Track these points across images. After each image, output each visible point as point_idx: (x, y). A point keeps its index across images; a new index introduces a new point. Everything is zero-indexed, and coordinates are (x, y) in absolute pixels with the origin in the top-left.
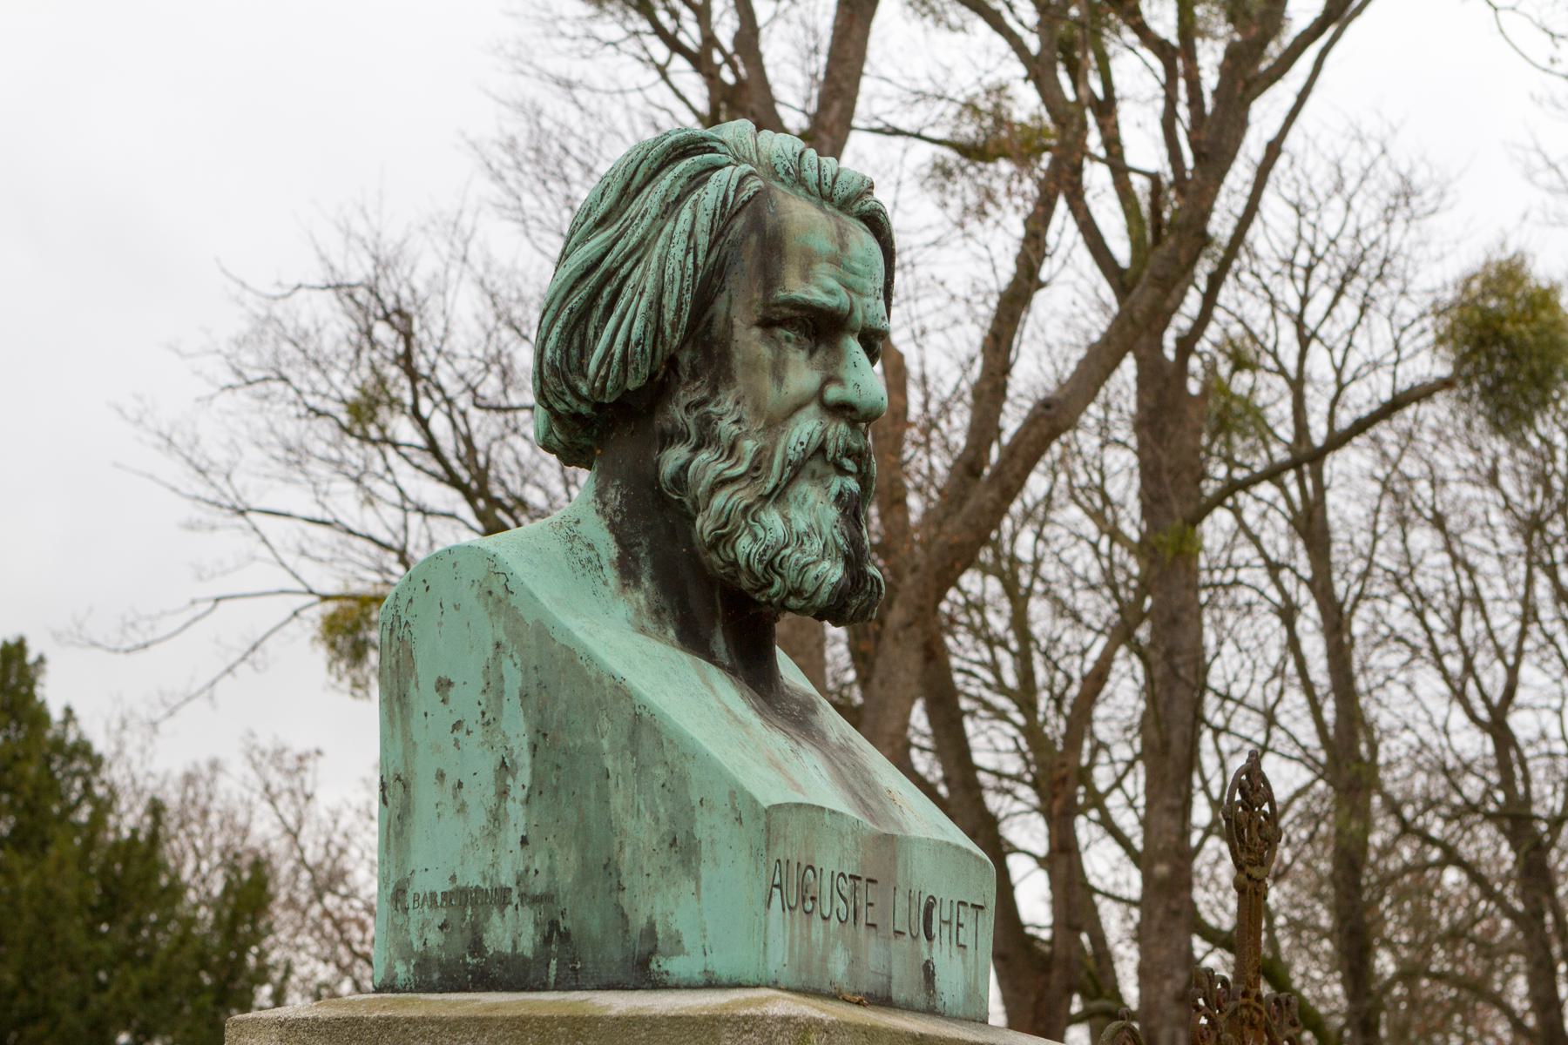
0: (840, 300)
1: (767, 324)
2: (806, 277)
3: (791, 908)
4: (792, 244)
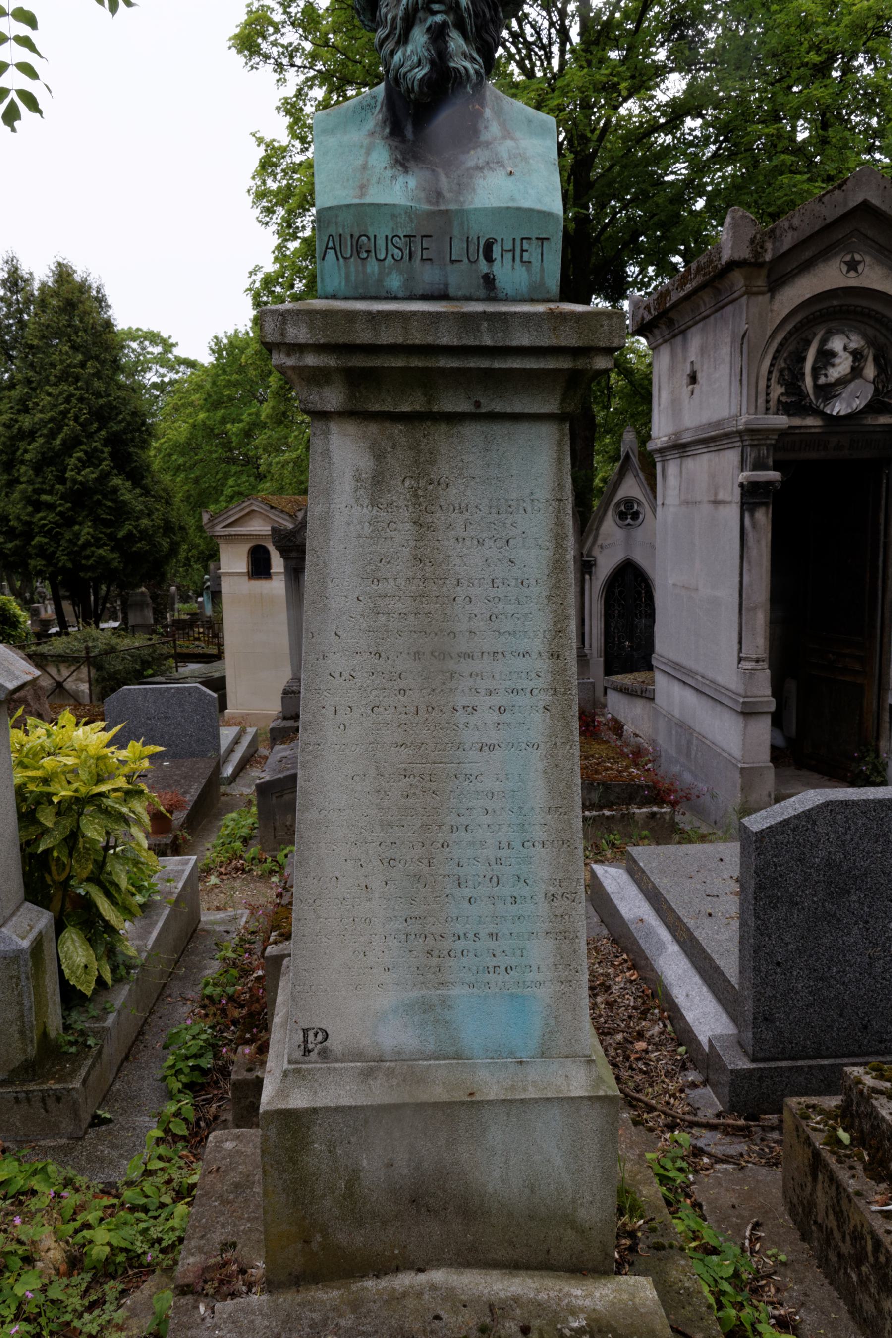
3: (345, 258)
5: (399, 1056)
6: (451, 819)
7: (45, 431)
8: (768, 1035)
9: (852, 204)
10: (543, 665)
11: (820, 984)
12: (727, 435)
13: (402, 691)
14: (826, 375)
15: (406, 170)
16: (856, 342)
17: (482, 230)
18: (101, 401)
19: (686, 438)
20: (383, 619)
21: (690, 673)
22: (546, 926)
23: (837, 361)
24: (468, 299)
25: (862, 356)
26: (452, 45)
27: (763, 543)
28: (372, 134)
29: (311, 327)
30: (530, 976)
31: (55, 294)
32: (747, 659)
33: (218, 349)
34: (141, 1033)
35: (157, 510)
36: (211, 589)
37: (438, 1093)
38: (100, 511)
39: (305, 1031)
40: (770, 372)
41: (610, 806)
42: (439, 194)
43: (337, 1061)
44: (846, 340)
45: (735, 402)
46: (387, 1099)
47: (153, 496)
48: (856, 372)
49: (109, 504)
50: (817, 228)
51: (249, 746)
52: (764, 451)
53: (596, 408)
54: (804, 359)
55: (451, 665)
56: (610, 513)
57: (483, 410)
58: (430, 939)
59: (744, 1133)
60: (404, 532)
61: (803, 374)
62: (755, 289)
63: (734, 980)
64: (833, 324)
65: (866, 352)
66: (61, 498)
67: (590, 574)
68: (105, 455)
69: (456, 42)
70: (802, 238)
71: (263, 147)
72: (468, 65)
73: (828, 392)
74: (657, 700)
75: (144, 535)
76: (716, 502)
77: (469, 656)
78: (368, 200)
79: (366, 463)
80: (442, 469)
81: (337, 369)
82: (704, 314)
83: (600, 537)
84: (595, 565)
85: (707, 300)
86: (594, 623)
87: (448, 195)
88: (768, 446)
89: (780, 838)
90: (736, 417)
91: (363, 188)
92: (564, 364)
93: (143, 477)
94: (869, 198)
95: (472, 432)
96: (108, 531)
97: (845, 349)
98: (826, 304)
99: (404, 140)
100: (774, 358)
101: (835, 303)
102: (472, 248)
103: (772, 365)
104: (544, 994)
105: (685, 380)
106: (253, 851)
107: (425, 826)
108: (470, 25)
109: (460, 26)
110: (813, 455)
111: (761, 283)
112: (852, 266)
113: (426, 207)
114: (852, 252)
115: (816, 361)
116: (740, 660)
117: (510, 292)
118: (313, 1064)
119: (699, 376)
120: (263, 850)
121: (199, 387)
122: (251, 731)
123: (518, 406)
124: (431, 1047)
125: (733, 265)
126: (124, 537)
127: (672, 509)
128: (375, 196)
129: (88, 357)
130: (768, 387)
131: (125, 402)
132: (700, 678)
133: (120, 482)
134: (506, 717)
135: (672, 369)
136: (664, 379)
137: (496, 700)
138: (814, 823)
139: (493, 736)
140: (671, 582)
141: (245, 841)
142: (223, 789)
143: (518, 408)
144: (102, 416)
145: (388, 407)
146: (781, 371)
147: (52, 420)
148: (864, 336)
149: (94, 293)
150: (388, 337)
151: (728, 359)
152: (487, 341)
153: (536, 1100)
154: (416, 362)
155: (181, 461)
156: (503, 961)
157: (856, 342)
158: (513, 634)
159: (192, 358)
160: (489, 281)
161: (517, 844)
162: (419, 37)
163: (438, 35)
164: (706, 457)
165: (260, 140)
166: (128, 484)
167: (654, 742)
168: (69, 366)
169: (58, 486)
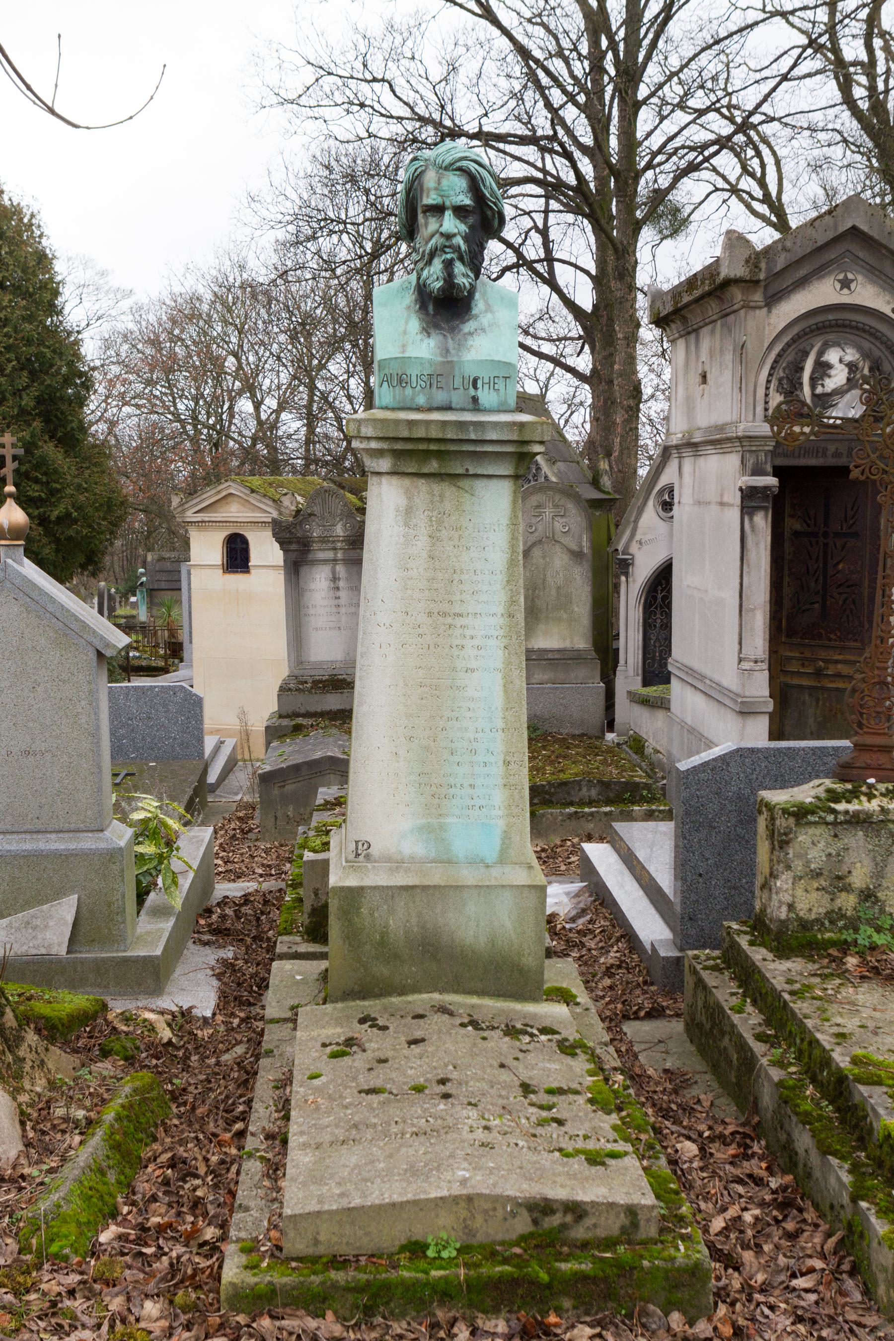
0: (439, 201)
1: (424, 212)
2: (428, 197)
4: (425, 187)
5: (412, 859)
8: (693, 932)
9: (842, 229)
11: (733, 892)
12: (729, 440)
13: (420, 635)
14: (823, 385)
15: (429, 335)
17: (471, 371)
18: (33, 349)
19: (698, 438)
20: (410, 592)
21: (702, 677)
23: (832, 372)
24: (463, 409)
25: (857, 369)
26: (456, 271)
27: (762, 546)
29: (375, 428)
39: (357, 842)
40: (768, 382)
41: (609, 802)
42: (447, 351)
43: (375, 861)
44: (842, 353)
48: (851, 383)
50: (809, 250)
54: (802, 369)
56: (651, 503)
57: (471, 473)
58: (434, 788)
60: (422, 544)
61: (801, 384)
62: (752, 304)
63: (672, 897)
64: (831, 337)
65: (861, 364)
67: (627, 575)
69: (459, 268)
72: (465, 281)
73: (824, 400)
74: (672, 709)
77: (460, 615)
78: (407, 355)
79: (402, 501)
81: (388, 450)
82: (712, 318)
84: (633, 564)
85: (714, 306)
86: (630, 633)
87: (453, 352)
90: (735, 424)
94: (857, 224)
97: (841, 361)
98: (820, 319)
99: (427, 314)
100: (772, 368)
101: (830, 317)
102: (466, 382)
103: (770, 375)
105: (699, 379)
107: (432, 717)
109: (461, 259)
113: (440, 359)
114: (845, 271)
115: (813, 372)
116: (740, 660)
119: (708, 376)
124: (433, 855)
125: (728, 283)
127: (687, 508)
128: (412, 352)
130: (767, 395)
132: (708, 682)
134: (481, 652)
137: (475, 642)
138: (728, 764)
146: (780, 380)
148: (860, 349)
151: (730, 366)
152: (473, 436)
153: (496, 887)
156: (477, 802)
157: (851, 355)
158: (487, 603)
160: (475, 400)
161: (487, 730)
162: (437, 266)
163: (448, 265)
164: (715, 457)
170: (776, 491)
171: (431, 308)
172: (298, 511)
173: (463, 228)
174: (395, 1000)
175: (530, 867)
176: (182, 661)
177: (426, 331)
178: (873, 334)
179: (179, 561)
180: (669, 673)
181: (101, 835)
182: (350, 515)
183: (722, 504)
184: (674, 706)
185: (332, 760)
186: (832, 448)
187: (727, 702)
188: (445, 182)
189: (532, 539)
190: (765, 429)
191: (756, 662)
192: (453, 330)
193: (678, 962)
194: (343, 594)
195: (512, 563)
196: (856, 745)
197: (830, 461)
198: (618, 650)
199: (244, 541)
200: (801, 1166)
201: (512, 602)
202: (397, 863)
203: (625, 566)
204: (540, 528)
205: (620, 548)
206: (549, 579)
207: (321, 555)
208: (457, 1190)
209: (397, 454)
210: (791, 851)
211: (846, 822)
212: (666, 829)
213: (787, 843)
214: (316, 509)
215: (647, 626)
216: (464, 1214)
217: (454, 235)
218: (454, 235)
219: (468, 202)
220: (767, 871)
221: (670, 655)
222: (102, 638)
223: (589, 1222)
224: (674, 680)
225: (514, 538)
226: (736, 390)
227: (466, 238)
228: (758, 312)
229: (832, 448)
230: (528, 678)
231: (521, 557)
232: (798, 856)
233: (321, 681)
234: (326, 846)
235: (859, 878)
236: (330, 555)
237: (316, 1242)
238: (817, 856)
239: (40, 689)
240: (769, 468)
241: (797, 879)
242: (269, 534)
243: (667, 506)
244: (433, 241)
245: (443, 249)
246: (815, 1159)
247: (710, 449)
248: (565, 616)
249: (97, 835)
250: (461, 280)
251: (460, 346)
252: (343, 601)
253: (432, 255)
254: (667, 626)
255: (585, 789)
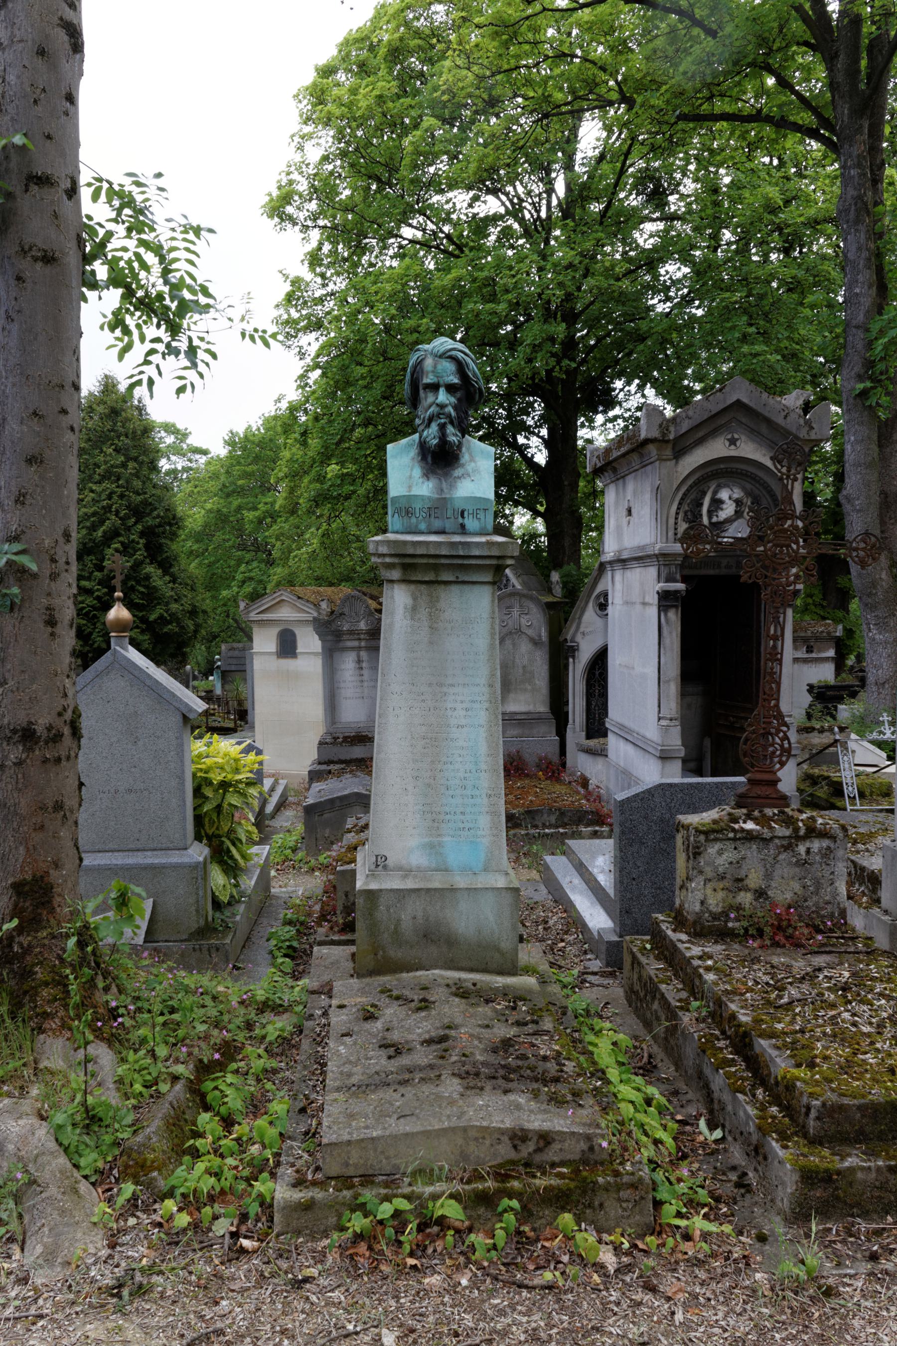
5: (419, 869)
6: (444, 759)
7: (88, 524)
8: (628, 922)
10: (486, 690)
12: (649, 556)
13: (423, 701)
16: (738, 494)
17: (460, 506)
19: (625, 555)
21: (630, 731)
22: (487, 809)
23: (724, 506)
24: (454, 533)
27: (674, 634)
28: (413, 459)
29: (389, 547)
30: (480, 833)
31: (101, 402)
32: (663, 718)
33: (231, 443)
34: (248, 938)
35: (185, 596)
36: (223, 669)
37: (436, 885)
38: (133, 596)
40: (677, 514)
41: (564, 825)
42: (442, 490)
45: (653, 533)
46: (416, 886)
47: (180, 584)
48: (738, 514)
49: (142, 589)
51: (282, 796)
52: (673, 569)
53: (583, 509)
54: (702, 504)
55: (445, 689)
56: (591, 604)
59: (612, 975)
63: (612, 895)
64: (722, 481)
66: (99, 584)
67: (573, 657)
68: (140, 546)
69: (450, 429)
70: (695, 423)
71: (288, 283)
73: (719, 526)
75: (174, 618)
76: (644, 604)
77: (453, 685)
79: (409, 601)
80: (442, 604)
83: (583, 625)
86: (577, 700)
88: (676, 565)
89: (634, 804)
91: (410, 487)
92: (494, 562)
93: (171, 566)
95: (455, 589)
96: (141, 614)
97: (730, 498)
98: (714, 467)
99: (427, 463)
100: (680, 504)
103: (678, 509)
104: (486, 841)
105: (625, 513)
106: (300, 855)
107: (433, 762)
108: (456, 422)
109: (452, 423)
110: (711, 572)
111: (668, 452)
112: (733, 442)
113: (436, 496)
115: (710, 506)
116: (659, 719)
117: (472, 530)
118: (380, 871)
120: (307, 854)
121: (215, 476)
122: (283, 782)
123: (475, 578)
125: (647, 441)
126: (155, 620)
127: (618, 607)
128: (415, 491)
129: (128, 459)
131: (160, 499)
133: (152, 570)
134: (469, 713)
135: (617, 503)
136: (612, 509)
137: (464, 705)
139: (463, 722)
140: (618, 662)
141: (294, 850)
142: (267, 822)
143: (475, 579)
144: (138, 512)
145: (419, 578)
146: (686, 513)
147: (94, 514)
148: (743, 489)
149: (136, 403)
150: (419, 551)
152: (461, 553)
154: (431, 561)
155: (195, 547)
156: (467, 825)
157: (738, 494)
158: (472, 676)
159: (204, 447)
160: (463, 526)
161: (474, 771)
162: (434, 428)
163: (442, 427)
164: (638, 570)
165: (286, 277)
166: (159, 572)
167: (608, 788)
168: (112, 466)
169: (96, 573)
170: (684, 594)
171: (429, 459)
172: (332, 612)
173: (453, 400)
174: (404, 975)
175: (507, 874)
176: (247, 723)
177: (426, 475)
178: (753, 478)
179: (244, 649)
180: (607, 729)
181: (185, 852)
182: (371, 614)
183: (644, 604)
184: (611, 753)
185: (358, 795)
186: (724, 562)
187: (650, 750)
188: (439, 367)
189: (505, 630)
190: (678, 548)
191: (671, 720)
192: (447, 475)
193: (618, 945)
194: (365, 672)
195: (492, 646)
196: (749, 780)
197: (724, 571)
198: (567, 713)
199: (293, 635)
200: (716, 1102)
201: (493, 675)
202: (406, 872)
203: (573, 651)
204: (510, 623)
205: (569, 637)
206: (517, 660)
207: (349, 644)
208: (454, 1122)
209: (405, 567)
210: (702, 861)
211: (745, 838)
212: (608, 844)
213: (699, 854)
214: (346, 610)
215: (589, 695)
216: (460, 1141)
217: (446, 406)
218: (446, 406)
219: (456, 381)
220: (684, 876)
221: (607, 716)
222: (187, 705)
223: (556, 1146)
224: (610, 735)
225: (493, 628)
226: (654, 520)
227: (455, 408)
228: (668, 463)
229: (724, 562)
230: (504, 732)
231: (497, 642)
232: (707, 864)
233: (349, 737)
234: (354, 861)
235: (754, 879)
236: (356, 644)
237: (347, 1165)
238: (722, 861)
239: (140, 743)
240: (678, 577)
241: (707, 880)
242: (311, 629)
243: (603, 606)
244: (431, 410)
245: (438, 416)
246: (726, 1097)
247: (635, 564)
248: (529, 687)
249: (182, 852)
250: (452, 439)
251: (452, 486)
252: (365, 677)
253: (430, 420)
254: (604, 695)
255: (545, 815)
